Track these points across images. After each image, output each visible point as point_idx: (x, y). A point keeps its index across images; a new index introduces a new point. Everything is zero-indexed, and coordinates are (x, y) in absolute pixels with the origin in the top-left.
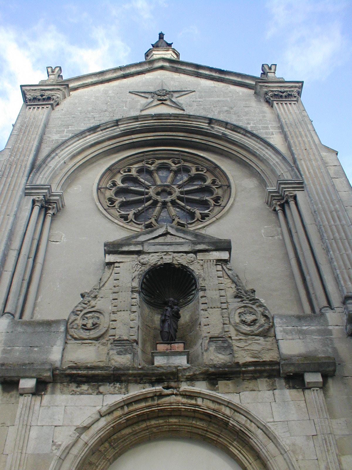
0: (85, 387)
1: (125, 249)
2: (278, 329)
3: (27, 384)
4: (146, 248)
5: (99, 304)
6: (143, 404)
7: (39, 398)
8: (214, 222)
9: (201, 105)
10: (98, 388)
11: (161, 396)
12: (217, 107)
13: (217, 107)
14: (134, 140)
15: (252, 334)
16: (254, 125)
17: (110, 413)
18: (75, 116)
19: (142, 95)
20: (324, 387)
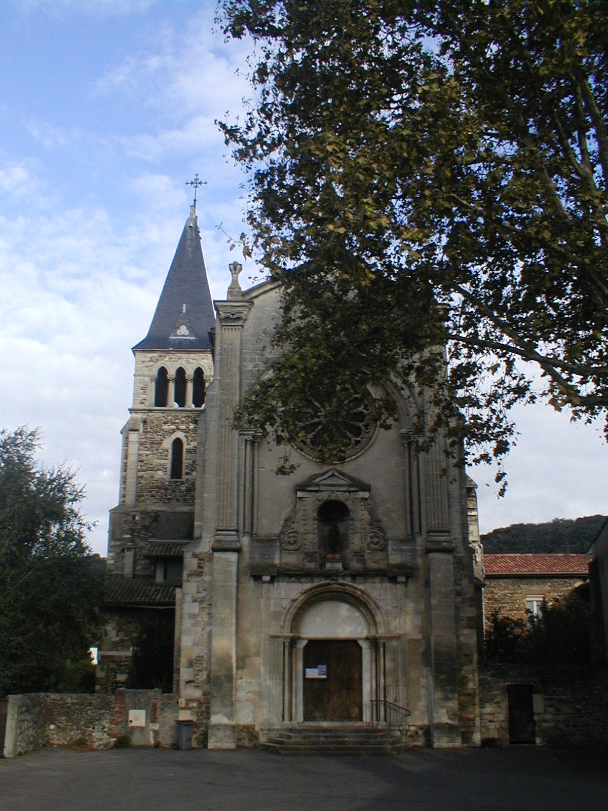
0: (293, 579)
1: (309, 489)
2: (390, 548)
3: (266, 578)
4: (322, 488)
5: (295, 527)
7: (271, 585)
8: (363, 454)
11: (329, 584)
15: (376, 550)
17: (306, 592)
20: (406, 583)
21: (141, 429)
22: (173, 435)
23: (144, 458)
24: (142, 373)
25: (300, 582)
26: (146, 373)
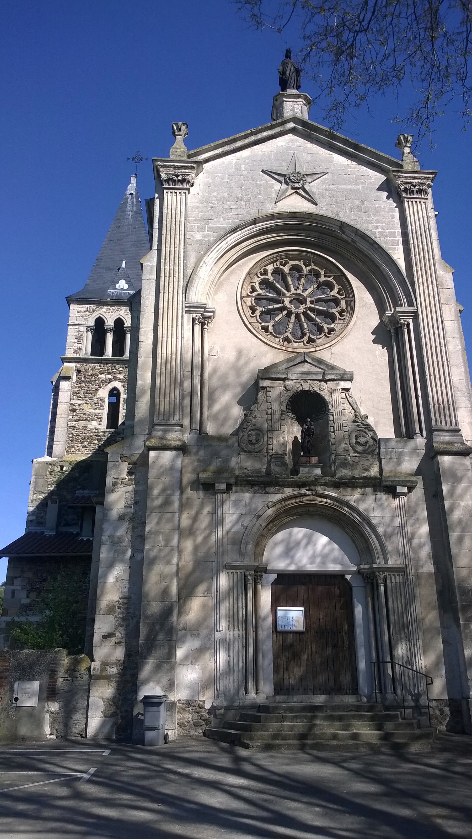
6: (294, 501)
9: (333, 196)
10: (265, 489)
12: (349, 199)
13: (349, 199)
14: (270, 240)
16: (382, 230)
18: (212, 205)
19: (276, 177)
21: (74, 378)
22: (109, 385)
23: (77, 407)
24: (77, 323)
25: (266, 493)
26: (82, 323)
